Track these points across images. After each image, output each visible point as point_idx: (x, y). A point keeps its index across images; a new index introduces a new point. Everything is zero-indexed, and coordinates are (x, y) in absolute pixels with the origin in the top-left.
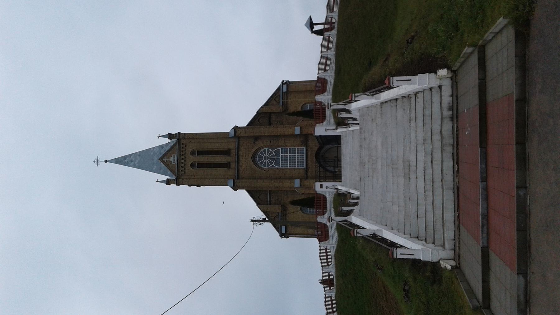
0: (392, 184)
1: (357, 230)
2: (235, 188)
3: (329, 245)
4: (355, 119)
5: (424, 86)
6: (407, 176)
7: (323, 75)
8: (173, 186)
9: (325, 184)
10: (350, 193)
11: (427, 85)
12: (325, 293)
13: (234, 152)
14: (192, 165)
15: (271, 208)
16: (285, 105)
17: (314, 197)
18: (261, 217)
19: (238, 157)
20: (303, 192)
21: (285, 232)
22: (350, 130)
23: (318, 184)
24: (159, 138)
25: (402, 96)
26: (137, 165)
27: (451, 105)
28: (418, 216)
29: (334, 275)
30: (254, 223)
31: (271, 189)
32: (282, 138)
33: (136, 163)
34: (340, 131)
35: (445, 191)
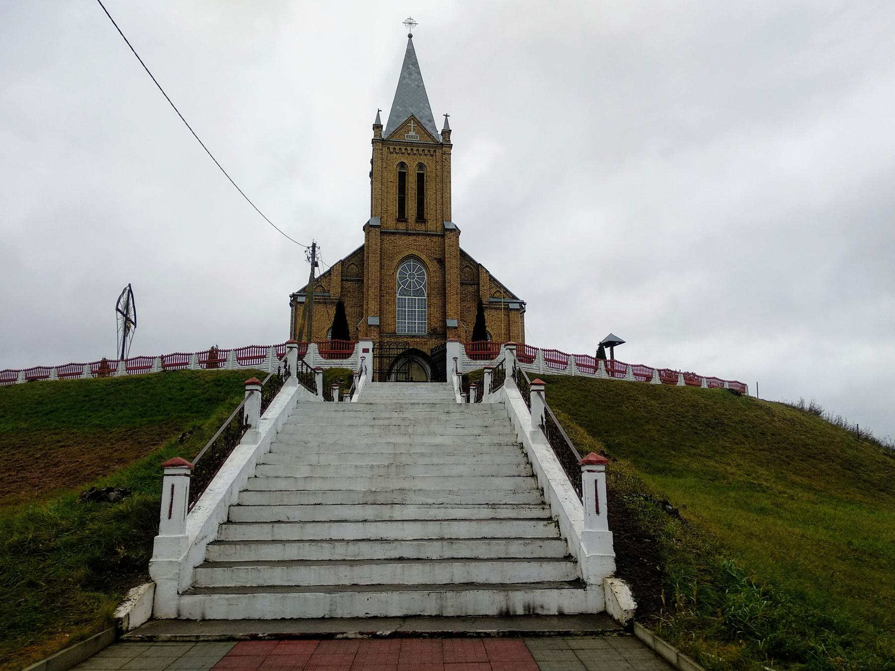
0: (356, 466)
1: (257, 390)
2: (368, 228)
3: (270, 362)
4: (479, 399)
5: (582, 545)
6: (371, 500)
7: (540, 356)
8: (371, 135)
9: (369, 356)
10: (353, 394)
11: (586, 553)
12: (195, 353)
13: (421, 228)
14: (402, 165)
15: (336, 279)
16: (493, 306)
17: (349, 340)
18: (320, 259)
19: (414, 234)
20: (359, 329)
21: (299, 302)
22: (455, 396)
23: (369, 345)
24: (444, 115)
25: (543, 488)
26: (404, 82)
27: (539, 611)
28: (276, 525)
29: (223, 368)
30: (311, 249)
31: (365, 282)
32: (441, 300)
33: (407, 80)
34: (454, 380)
35: (327, 595)
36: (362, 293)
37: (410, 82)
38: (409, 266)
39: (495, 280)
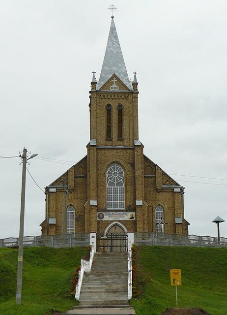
2: (89, 146)
13: (120, 145)
14: (109, 105)
15: (71, 177)
23: (94, 235)
36: (87, 184)
37: (112, 50)
38: (114, 168)
39: (165, 174)
